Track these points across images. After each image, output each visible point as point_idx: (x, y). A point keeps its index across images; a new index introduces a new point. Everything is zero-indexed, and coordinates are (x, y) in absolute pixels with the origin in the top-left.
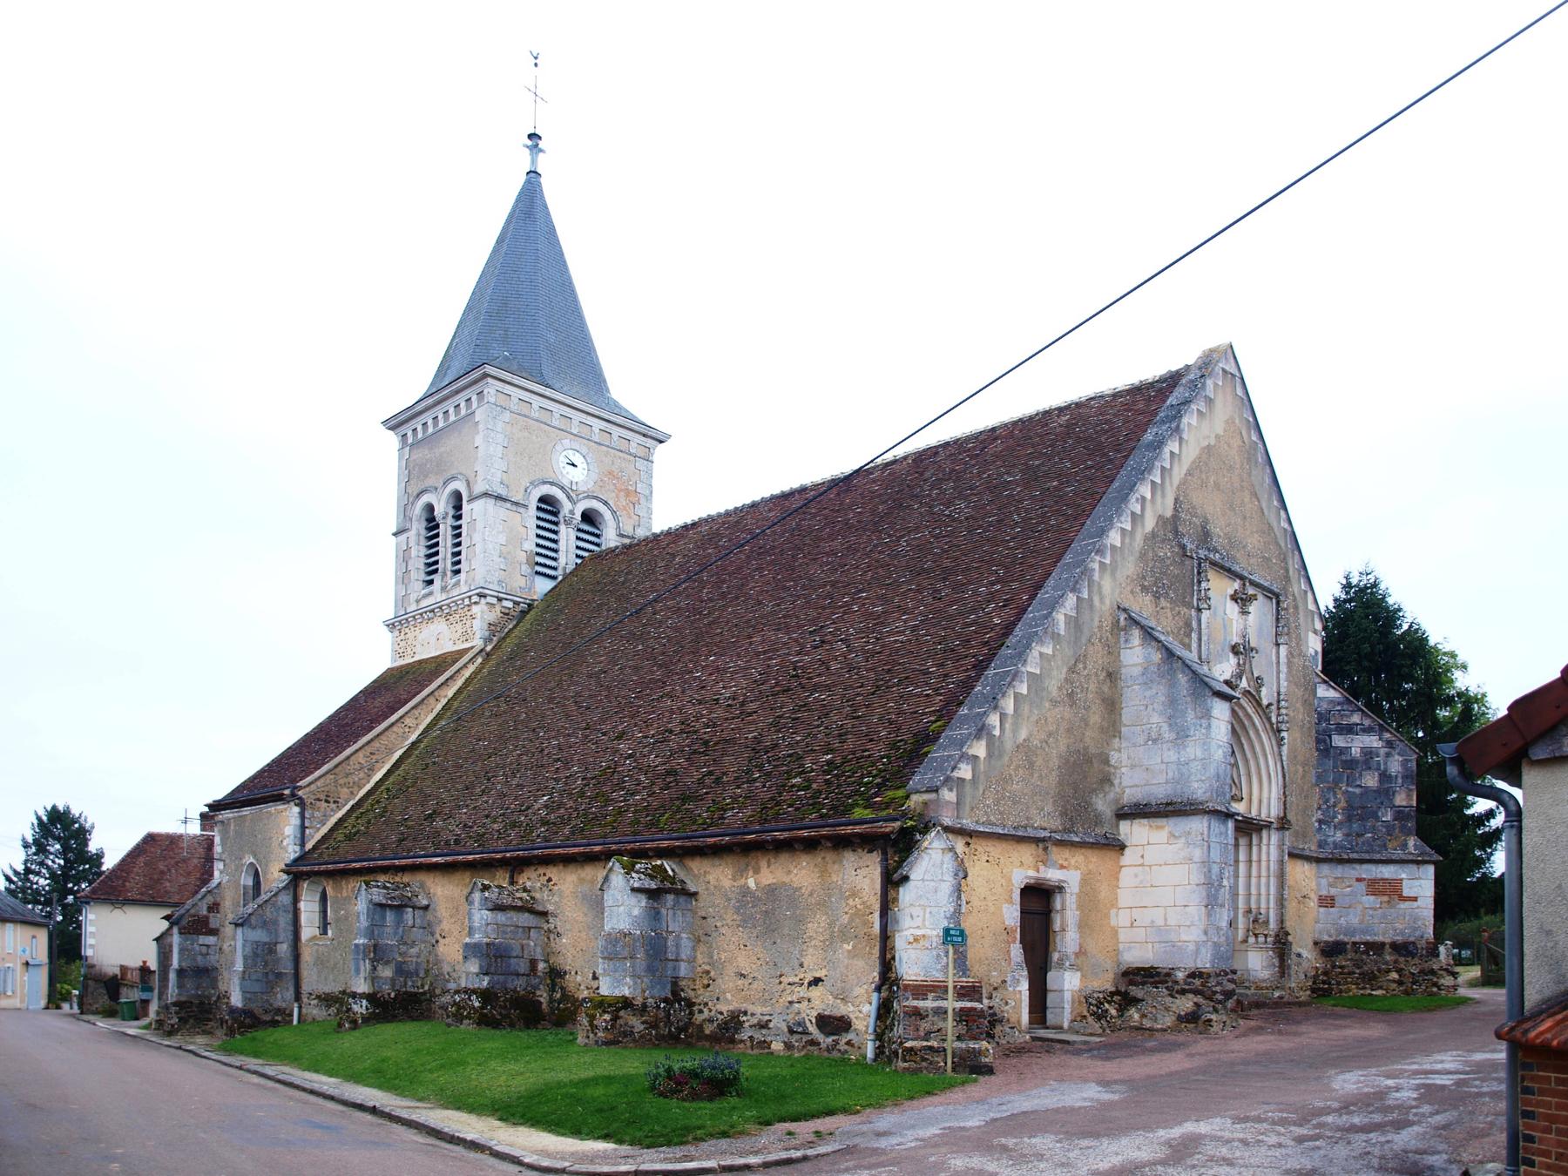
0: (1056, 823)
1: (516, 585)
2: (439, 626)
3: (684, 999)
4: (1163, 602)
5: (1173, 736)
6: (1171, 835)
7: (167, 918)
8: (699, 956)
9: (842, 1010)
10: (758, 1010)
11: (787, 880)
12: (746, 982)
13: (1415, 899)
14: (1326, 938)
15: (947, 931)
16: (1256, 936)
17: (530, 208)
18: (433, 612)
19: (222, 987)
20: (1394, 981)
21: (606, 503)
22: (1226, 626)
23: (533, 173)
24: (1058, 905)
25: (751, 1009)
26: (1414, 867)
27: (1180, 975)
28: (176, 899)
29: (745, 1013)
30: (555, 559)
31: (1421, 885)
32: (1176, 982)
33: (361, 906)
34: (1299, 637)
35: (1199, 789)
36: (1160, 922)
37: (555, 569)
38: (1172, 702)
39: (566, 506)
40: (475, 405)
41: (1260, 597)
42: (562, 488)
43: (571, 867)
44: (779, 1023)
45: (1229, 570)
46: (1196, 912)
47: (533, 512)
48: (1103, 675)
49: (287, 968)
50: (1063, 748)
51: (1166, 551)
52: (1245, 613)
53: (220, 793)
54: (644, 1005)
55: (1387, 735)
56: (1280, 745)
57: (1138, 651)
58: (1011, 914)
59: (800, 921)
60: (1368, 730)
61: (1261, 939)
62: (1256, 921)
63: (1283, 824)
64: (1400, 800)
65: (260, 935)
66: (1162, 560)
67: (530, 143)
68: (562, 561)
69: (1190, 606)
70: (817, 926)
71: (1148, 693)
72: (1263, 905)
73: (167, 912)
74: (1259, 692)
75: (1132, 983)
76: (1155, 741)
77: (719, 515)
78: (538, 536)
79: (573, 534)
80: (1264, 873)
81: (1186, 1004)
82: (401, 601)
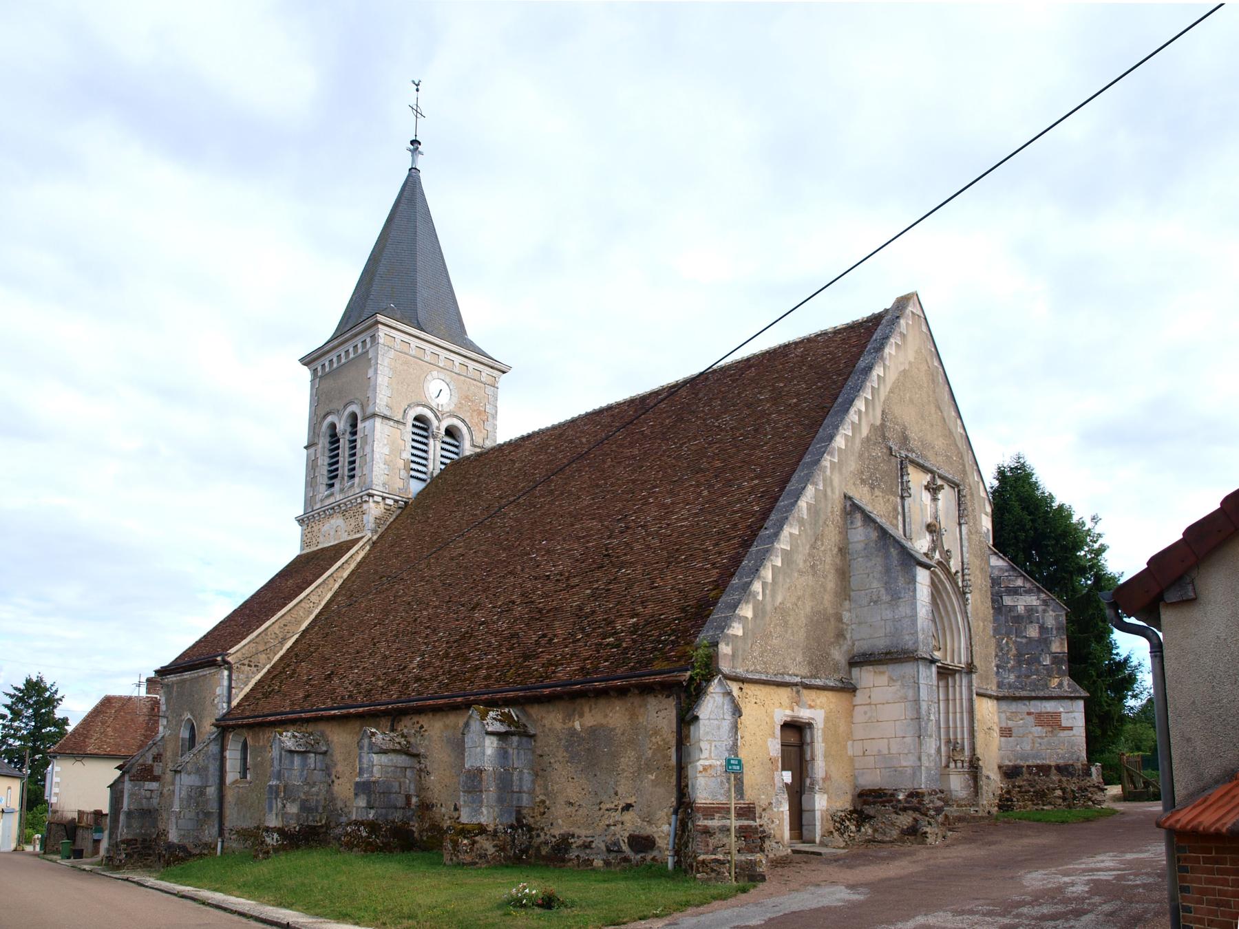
1: (396, 486)
2: (337, 521)
4: (877, 492)
5: (889, 598)
6: (891, 679)
9: (648, 830)
10: (583, 832)
11: (604, 722)
12: (573, 809)
14: (1007, 763)
15: (728, 761)
16: (955, 761)
17: (409, 206)
19: (161, 826)
20: (1059, 797)
21: (463, 421)
23: (413, 171)
24: (808, 740)
25: (577, 832)
26: (1069, 703)
29: (573, 836)
38: (888, 570)
39: (435, 423)
40: (368, 346)
41: (946, 487)
42: (431, 409)
43: (438, 716)
44: (599, 844)
47: (409, 428)
49: (213, 807)
50: (808, 609)
51: (878, 452)
52: (935, 499)
54: (495, 831)
58: (774, 747)
60: (1028, 592)
61: (959, 764)
62: (954, 747)
66: (875, 459)
68: (431, 467)
70: (628, 759)
71: (869, 564)
72: (959, 737)
74: (948, 563)
75: (865, 803)
76: (876, 602)
77: (548, 429)
79: (439, 445)
82: (309, 501)
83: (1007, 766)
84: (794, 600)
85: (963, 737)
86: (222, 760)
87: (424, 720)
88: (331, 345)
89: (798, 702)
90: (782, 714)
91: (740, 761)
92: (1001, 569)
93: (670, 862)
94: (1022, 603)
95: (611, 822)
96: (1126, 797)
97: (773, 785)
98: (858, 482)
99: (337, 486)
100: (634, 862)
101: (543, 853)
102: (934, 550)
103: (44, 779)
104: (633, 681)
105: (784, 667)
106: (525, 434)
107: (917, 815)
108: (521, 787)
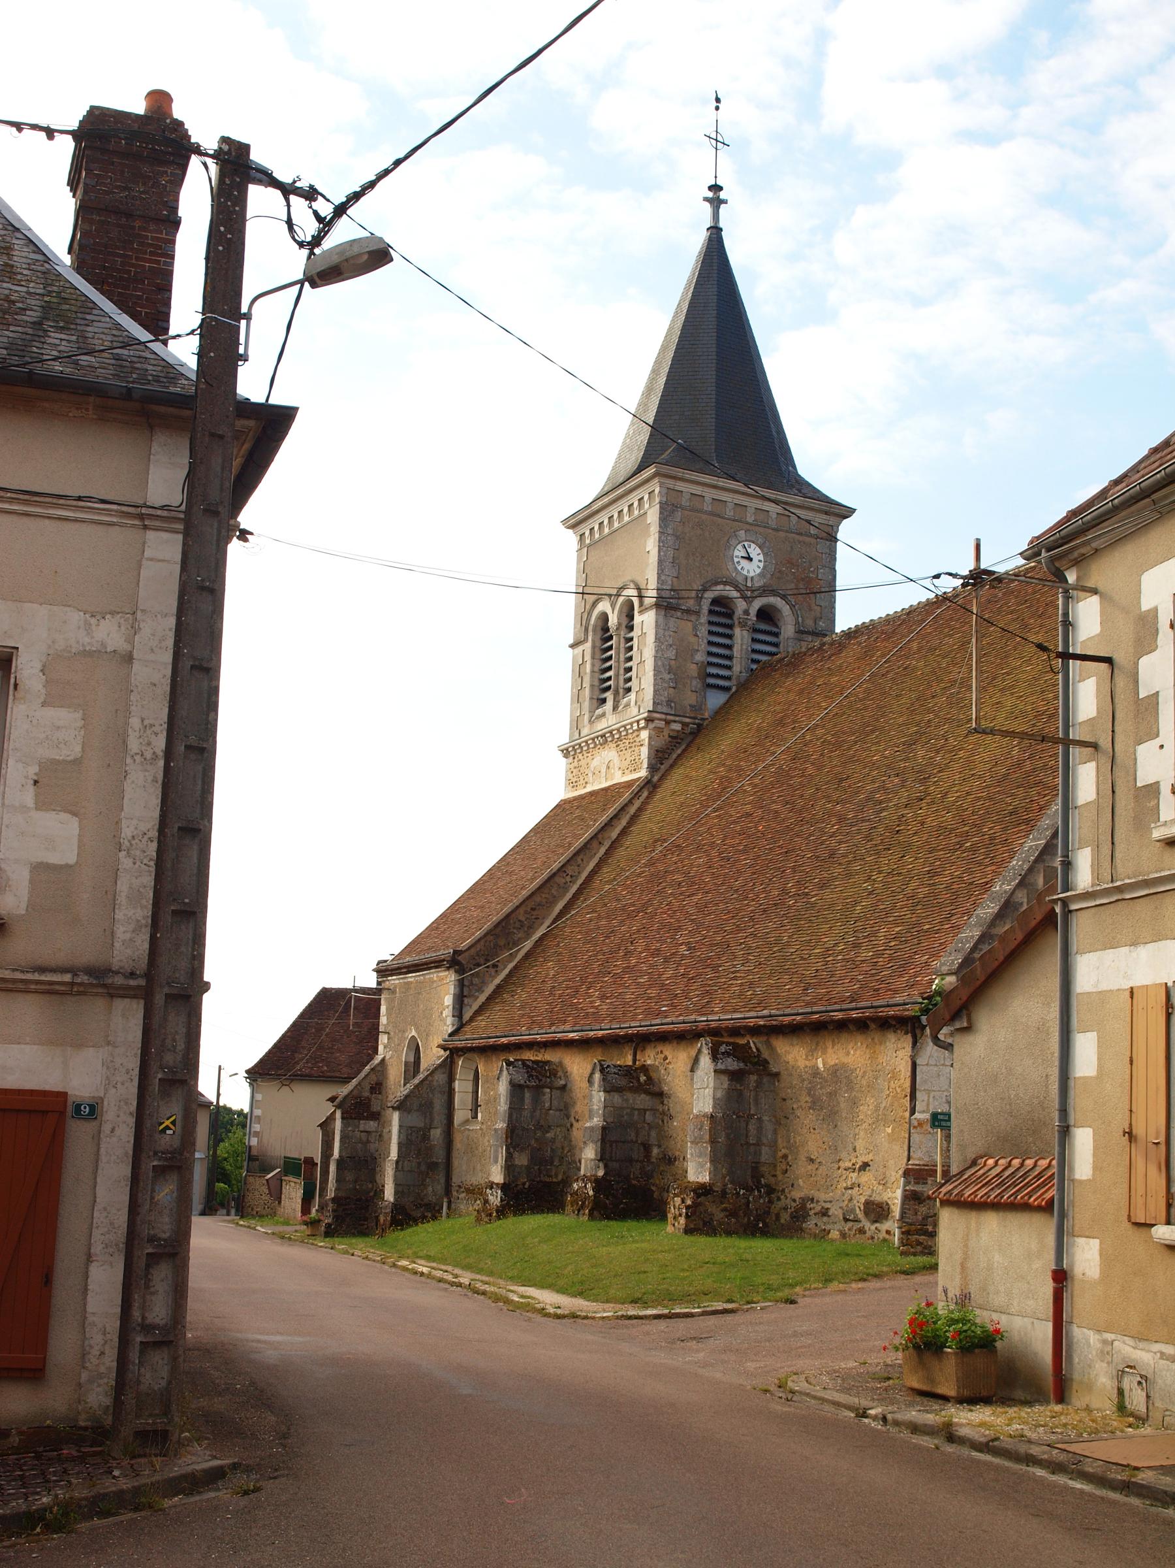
3: (767, 1186)
7: (332, 1099)
8: (780, 1141)
10: (822, 1196)
11: (845, 1060)
18: (604, 739)
23: (715, 232)
28: (346, 1071)
29: (812, 1200)
30: (729, 668)
33: (503, 1087)
37: (729, 678)
39: (741, 605)
40: (647, 506)
44: (836, 1211)
47: (704, 619)
49: (439, 1156)
53: (392, 946)
54: (724, 1193)
59: (854, 1103)
65: (416, 1120)
67: (710, 195)
68: (737, 668)
70: (867, 1108)
78: (710, 643)
82: (576, 724)
86: (451, 1093)
87: (668, 1050)
88: (600, 504)
99: (610, 704)
100: (868, 1234)
101: (782, 1221)
103: (657, 651)
108: (759, 1139)
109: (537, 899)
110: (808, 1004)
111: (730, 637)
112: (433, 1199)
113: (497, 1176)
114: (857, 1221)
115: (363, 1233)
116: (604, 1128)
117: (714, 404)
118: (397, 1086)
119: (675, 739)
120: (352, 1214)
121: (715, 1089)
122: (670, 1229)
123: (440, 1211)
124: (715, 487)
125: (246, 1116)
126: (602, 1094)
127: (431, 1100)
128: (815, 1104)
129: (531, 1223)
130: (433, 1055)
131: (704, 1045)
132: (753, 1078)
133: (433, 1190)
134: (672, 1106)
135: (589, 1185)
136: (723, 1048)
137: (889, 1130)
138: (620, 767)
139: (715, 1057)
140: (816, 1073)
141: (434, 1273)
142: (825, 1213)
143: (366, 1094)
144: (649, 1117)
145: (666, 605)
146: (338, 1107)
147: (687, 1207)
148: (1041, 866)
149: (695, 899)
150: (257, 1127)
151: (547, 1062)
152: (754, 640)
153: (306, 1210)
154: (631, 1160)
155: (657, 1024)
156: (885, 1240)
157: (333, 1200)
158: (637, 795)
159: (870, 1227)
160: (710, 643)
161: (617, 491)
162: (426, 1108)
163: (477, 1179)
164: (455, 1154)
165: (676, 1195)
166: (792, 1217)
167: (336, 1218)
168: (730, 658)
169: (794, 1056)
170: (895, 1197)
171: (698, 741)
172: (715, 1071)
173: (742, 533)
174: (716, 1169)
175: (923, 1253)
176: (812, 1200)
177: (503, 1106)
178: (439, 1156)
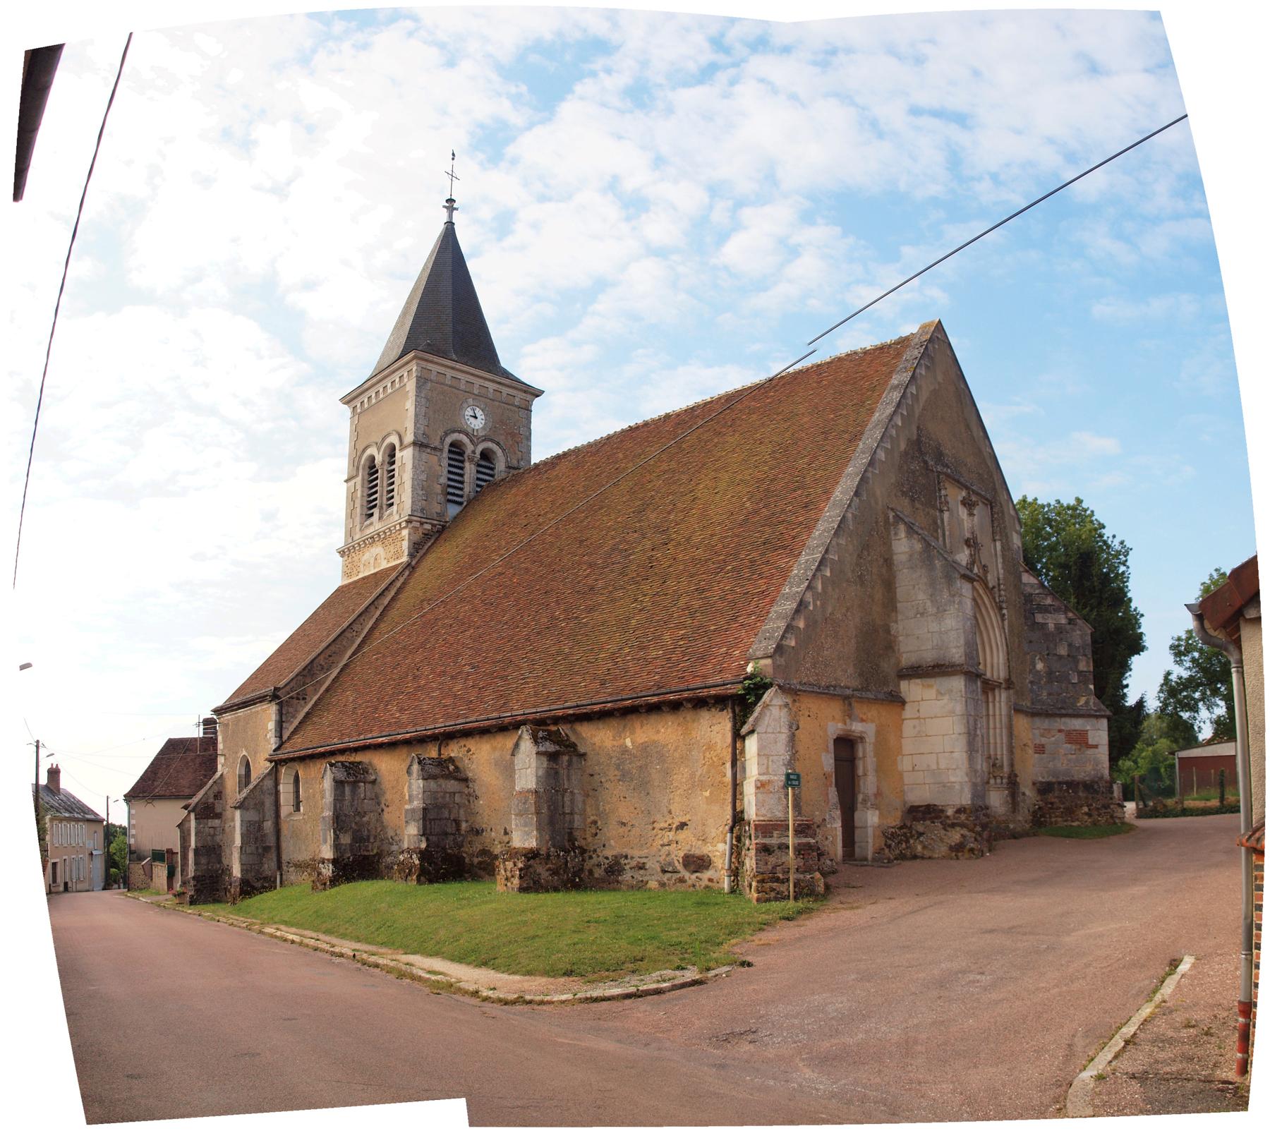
0: (855, 683)
2: (378, 550)
3: (580, 847)
4: (917, 505)
6: (939, 693)
7: (186, 807)
9: (706, 850)
10: (636, 853)
11: (655, 738)
12: (626, 829)
13: (1096, 747)
15: (788, 775)
18: (372, 540)
20: (1086, 814)
21: (498, 444)
22: (960, 522)
24: (860, 754)
25: (630, 852)
26: (1094, 721)
27: (950, 812)
28: (187, 792)
29: (626, 857)
30: (461, 489)
31: (1099, 734)
32: (948, 817)
33: (328, 784)
34: (1007, 536)
35: (956, 654)
36: (934, 767)
37: (461, 496)
38: (932, 583)
39: (469, 448)
42: (467, 434)
43: (486, 737)
44: (652, 865)
45: (958, 481)
46: (960, 755)
47: (445, 454)
48: (881, 561)
49: (271, 841)
51: (915, 466)
52: (971, 514)
53: (220, 702)
54: (548, 855)
55: (1070, 615)
56: (1003, 620)
57: (905, 540)
58: (828, 762)
59: (667, 773)
60: (1057, 610)
61: (999, 781)
62: (995, 765)
63: (1009, 684)
64: (1083, 666)
65: (253, 816)
66: (913, 472)
69: (934, 507)
70: (681, 776)
73: (183, 803)
75: (915, 819)
76: (922, 614)
77: (583, 447)
78: (450, 472)
79: (474, 468)
80: (998, 725)
81: (955, 836)
82: (350, 533)
83: (1041, 783)
84: (844, 610)
85: (1002, 753)
86: (277, 793)
87: (471, 743)
88: (369, 383)
89: (849, 715)
90: (835, 728)
91: (798, 776)
92: (1032, 586)
93: (726, 886)
94: (1052, 621)
95: (666, 841)
96: (1141, 814)
97: (827, 801)
98: (899, 494)
99: (376, 516)
100: (690, 882)
101: (596, 875)
102: (973, 563)
104: (686, 695)
105: (836, 679)
106: (560, 452)
107: (964, 831)
108: (573, 809)
109: (332, 648)
110: (610, 695)
111: (462, 468)
112: (269, 873)
113: (327, 853)
114: (675, 872)
115: (217, 901)
116: (424, 809)
117: (448, 319)
118: (233, 793)
119: (427, 536)
120: (208, 888)
121: (537, 768)
122: (500, 887)
123: (275, 881)
124: (453, 368)
125: (125, 828)
126: (421, 782)
127: (263, 801)
128: (625, 776)
129: (365, 889)
130: (261, 767)
131: (525, 734)
132: (566, 758)
133: (269, 866)
134: (477, 788)
135: (414, 856)
136: (541, 734)
137: (707, 794)
138: (383, 558)
139: (536, 740)
140: (625, 750)
141: (306, 941)
142: (641, 867)
143: (211, 800)
144: (457, 798)
145: (419, 445)
146: (193, 810)
147: (521, 870)
148: (819, 574)
149: (468, 633)
150: (133, 832)
151: (360, 763)
152: (478, 472)
153: (170, 886)
154: (446, 834)
155: (460, 723)
156: (707, 887)
157: (194, 878)
158: (401, 574)
159: (691, 877)
160: (450, 472)
161: (382, 373)
162: (259, 806)
163: (304, 856)
164: (283, 838)
165: (505, 860)
166: (606, 871)
167: (197, 891)
168: (462, 483)
169: (600, 739)
170: (719, 850)
171: (443, 536)
172: (537, 753)
173: (470, 401)
174: (541, 836)
175: (776, 899)
176: (626, 857)
177: (329, 798)
178: (271, 841)
